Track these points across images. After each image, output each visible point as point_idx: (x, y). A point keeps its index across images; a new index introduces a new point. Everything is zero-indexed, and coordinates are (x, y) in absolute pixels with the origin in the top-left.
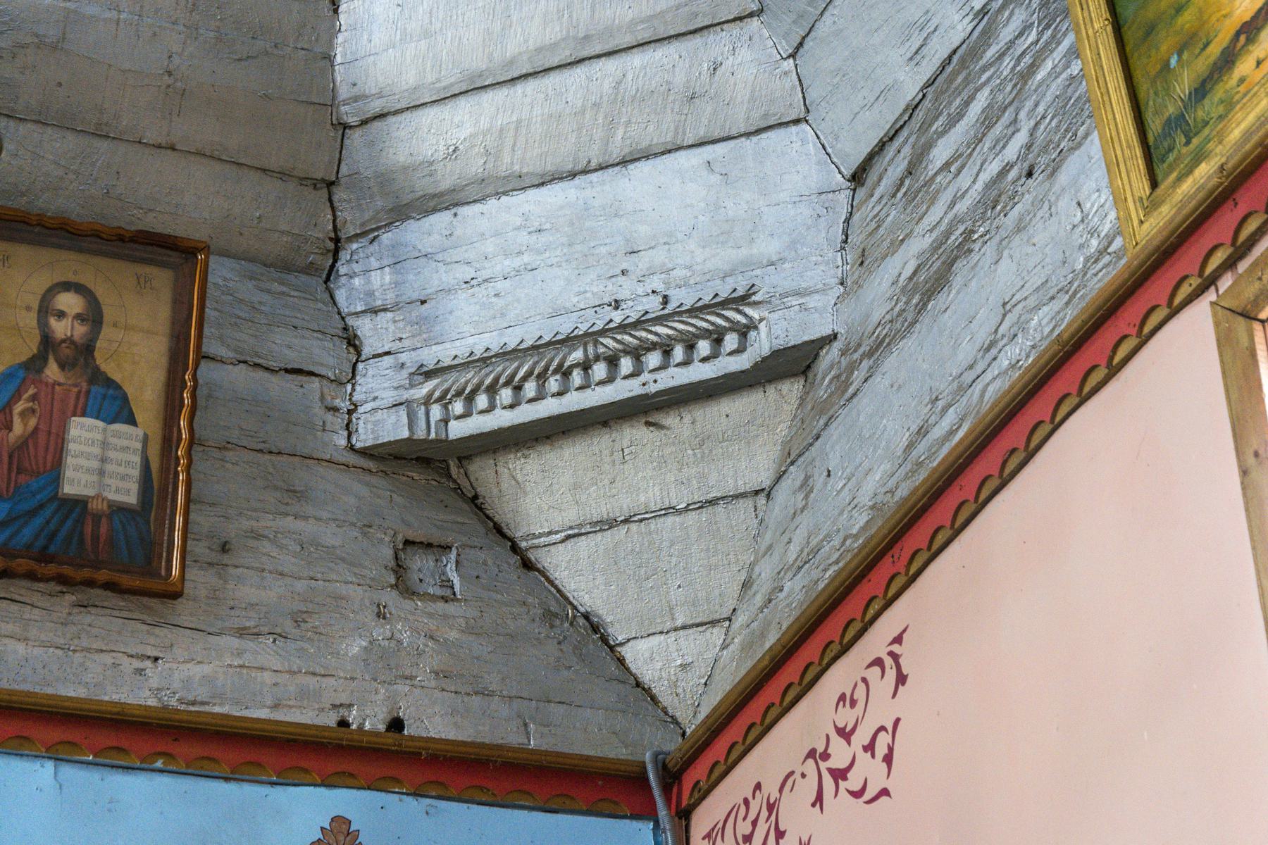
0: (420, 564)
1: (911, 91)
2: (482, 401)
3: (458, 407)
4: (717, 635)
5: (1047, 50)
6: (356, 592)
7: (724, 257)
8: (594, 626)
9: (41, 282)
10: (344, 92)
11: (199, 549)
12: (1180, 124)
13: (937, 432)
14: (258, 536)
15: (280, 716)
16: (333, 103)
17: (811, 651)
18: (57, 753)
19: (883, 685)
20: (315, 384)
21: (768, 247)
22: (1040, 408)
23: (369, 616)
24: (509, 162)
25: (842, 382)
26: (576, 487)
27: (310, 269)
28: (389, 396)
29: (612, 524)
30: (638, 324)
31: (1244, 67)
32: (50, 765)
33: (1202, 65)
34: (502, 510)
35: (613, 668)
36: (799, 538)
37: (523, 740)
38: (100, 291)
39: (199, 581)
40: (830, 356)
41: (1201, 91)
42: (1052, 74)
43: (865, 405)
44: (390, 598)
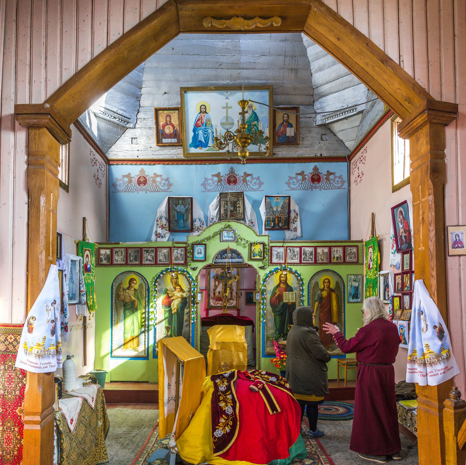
0: (324, 137)
2: (329, 119)
3: (327, 120)
4: (354, 141)
7: (353, 100)
9: (282, 114)
13: (372, 124)
14: (307, 136)
20: (312, 119)
21: (359, 99)
23: (318, 144)
24: (331, 91)
27: (311, 105)
28: (320, 119)
29: (343, 130)
32: (287, 164)
34: (332, 129)
35: (344, 146)
37: (333, 154)
38: (288, 114)
39: (301, 142)
40: (364, 111)
44: (321, 141)
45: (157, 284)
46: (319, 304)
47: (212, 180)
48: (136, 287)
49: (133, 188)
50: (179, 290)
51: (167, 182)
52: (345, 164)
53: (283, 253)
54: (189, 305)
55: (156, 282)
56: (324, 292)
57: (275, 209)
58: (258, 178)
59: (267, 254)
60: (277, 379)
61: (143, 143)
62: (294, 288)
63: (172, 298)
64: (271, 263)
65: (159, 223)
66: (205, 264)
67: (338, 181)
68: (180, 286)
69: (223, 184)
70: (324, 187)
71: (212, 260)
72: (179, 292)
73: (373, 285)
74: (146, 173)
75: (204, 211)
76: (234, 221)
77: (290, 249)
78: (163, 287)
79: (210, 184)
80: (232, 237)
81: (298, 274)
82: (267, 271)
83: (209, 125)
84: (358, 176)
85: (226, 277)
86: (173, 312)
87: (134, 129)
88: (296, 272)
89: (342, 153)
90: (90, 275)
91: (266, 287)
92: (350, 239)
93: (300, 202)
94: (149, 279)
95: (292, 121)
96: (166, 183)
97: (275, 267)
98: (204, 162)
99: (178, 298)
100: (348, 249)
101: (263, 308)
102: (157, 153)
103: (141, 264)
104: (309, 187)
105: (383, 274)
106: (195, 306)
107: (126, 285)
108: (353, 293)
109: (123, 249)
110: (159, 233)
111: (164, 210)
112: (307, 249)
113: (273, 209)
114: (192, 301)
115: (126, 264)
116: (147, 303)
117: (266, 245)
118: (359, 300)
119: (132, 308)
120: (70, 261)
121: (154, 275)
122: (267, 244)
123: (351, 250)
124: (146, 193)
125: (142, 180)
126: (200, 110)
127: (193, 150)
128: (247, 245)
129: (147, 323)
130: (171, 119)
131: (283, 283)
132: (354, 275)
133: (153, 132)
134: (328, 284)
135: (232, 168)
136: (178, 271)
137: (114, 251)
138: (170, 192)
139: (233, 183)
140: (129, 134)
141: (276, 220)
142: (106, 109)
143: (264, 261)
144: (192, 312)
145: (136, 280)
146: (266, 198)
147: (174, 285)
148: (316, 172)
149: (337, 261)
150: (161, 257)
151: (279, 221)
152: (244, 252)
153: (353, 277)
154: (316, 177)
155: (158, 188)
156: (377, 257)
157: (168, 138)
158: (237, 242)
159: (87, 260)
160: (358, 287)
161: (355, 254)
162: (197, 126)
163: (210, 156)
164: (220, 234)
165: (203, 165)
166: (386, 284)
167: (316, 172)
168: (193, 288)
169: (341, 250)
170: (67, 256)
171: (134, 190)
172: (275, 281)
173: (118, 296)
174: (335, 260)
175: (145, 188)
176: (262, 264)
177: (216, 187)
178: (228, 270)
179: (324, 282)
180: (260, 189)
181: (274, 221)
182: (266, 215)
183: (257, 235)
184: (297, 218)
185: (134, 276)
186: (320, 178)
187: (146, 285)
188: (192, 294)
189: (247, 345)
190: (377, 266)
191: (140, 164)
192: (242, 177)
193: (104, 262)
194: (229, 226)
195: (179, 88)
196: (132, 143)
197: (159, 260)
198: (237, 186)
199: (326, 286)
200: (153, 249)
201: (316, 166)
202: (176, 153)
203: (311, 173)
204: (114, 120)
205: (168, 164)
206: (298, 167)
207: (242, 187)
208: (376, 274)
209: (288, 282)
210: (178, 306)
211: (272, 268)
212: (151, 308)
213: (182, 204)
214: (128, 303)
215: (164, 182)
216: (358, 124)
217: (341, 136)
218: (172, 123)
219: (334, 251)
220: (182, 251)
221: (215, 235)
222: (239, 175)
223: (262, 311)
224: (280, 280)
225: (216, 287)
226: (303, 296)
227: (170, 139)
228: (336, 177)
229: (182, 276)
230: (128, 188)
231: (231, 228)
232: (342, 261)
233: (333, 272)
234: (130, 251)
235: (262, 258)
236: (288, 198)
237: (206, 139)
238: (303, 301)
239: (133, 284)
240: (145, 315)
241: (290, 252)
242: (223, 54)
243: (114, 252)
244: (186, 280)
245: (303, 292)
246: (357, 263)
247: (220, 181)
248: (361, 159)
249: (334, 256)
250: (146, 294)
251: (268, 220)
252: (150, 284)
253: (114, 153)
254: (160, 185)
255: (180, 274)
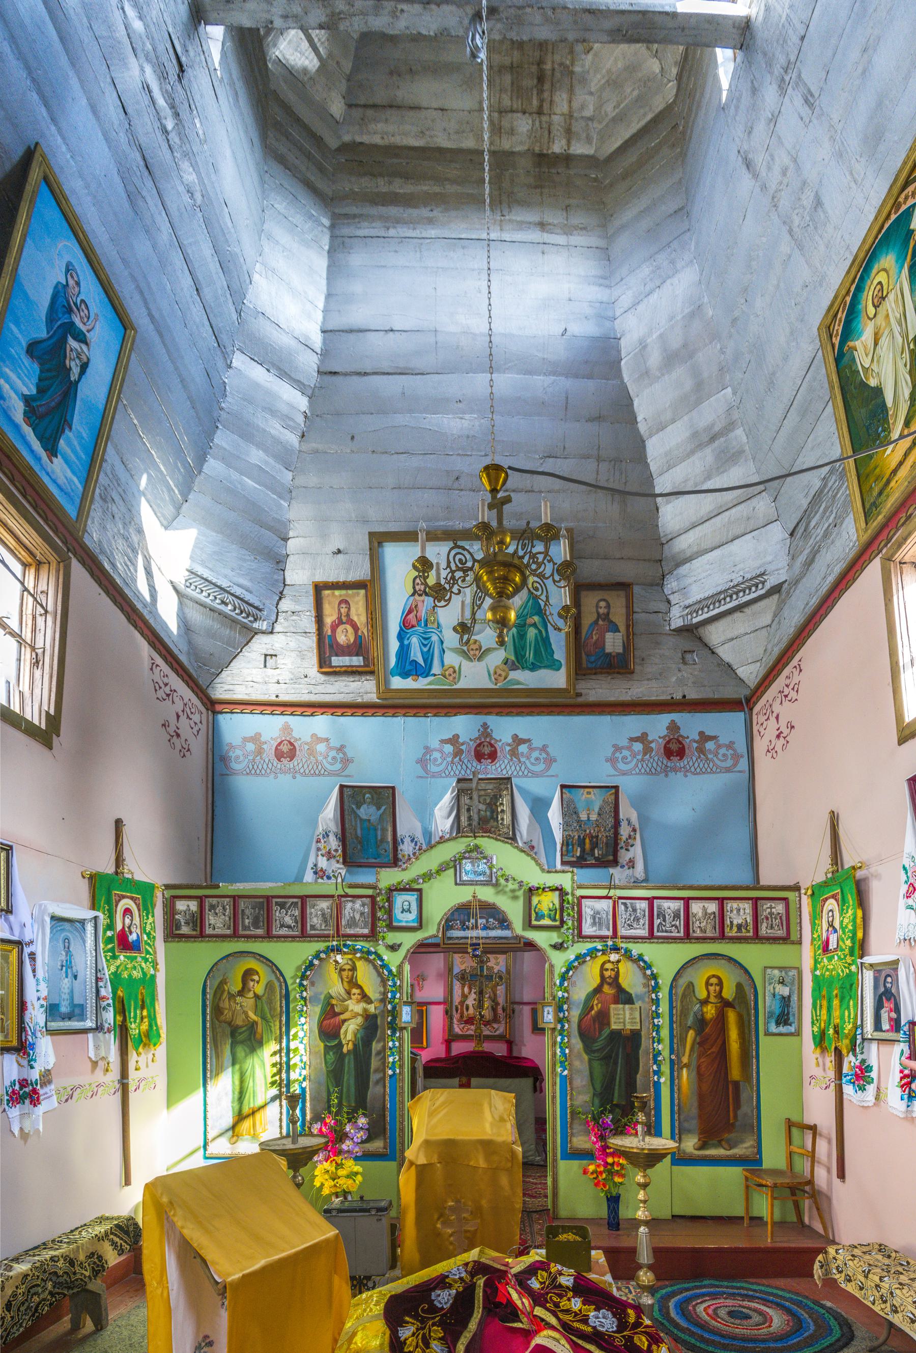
0: (688, 656)
1: (805, 507)
2: (700, 612)
3: (695, 615)
4: (758, 664)
5: (841, 487)
6: (674, 666)
8: (729, 666)
10: (662, 535)
11: (637, 661)
12: (875, 505)
13: (811, 604)
14: (649, 655)
15: (658, 698)
16: (659, 538)
17: (780, 666)
18: (610, 713)
19: (796, 672)
20: (661, 615)
21: (769, 558)
22: (836, 594)
25: (788, 593)
26: (724, 631)
27: (657, 585)
28: (678, 615)
29: (732, 639)
30: (737, 585)
31: (893, 484)
33: (881, 484)
34: (706, 640)
36: (777, 637)
39: (638, 668)
40: (785, 586)
41: (880, 493)
42: (843, 494)
43: (793, 598)
44: (681, 666)
45: (305, 983)
46: (696, 1035)
47: (441, 751)
48: (259, 989)
49: (265, 766)
50: (359, 997)
51: (341, 755)
52: (739, 717)
53: (607, 914)
54: (384, 1033)
55: (303, 977)
56: (709, 1007)
57: (583, 817)
58: (544, 749)
59: (569, 915)
60: (619, 1320)
61: (290, 666)
62: (637, 996)
63: (342, 1017)
64: (581, 936)
65: (321, 845)
66: (418, 936)
67: (724, 755)
68: (360, 987)
69: (466, 761)
70: (693, 769)
71: (435, 927)
72: (359, 1001)
73: (842, 993)
74: (295, 734)
75: (421, 821)
76: (489, 837)
77: (625, 904)
78: (320, 990)
79: (436, 760)
80: (484, 873)
81: (645, 962)
82: (570, 955)
83: (433, 623)
84: (778, 736)
85: (481, 976)
86: (345, 1050)
87: (271, 636)
88: (640, 958)
89: (729, 692)
90: (139, 959)
91: (567, 991)
92: (758, 882)
93: (640, 803)
94: (289, 971)
95: (619, 616)
96: (338, 757)
97: (589, 946)
98: (422, 712)
99: (356, 1015)
100: (765, 907)
101: (561, 1043)
102: (320, 689)
103: (269, 936)
104: (659, 769)
105: (871, 965)
106: (397, 1035)
107: (235, 985)
108: (777, 1011)
109: (228, 899)
110: (322, 870)
111: (331, 815)
112: (666, 904)
113: (578, 817)
114: (389, 1023)
115: (235, 935)
116: (284, 1029)
117: (567, 894)
118: (792, 1029)
119: (250, 1039)
120: (48, 919)
121: (300, 963)
122: (569, 890)
123: (771, 908)
124: (294, 778)
125: (285, 748)
126: (414, 588)
127: (397, 683)
128: (520, 893)
129: (284, 1076)
130: (349, 609)
131: (609, 984)
132: (780, 969)
133: (311, 642)
134: (718, 988)
135: (485, 726)
136: (355, 951)
137: (207, 904)
138: (346, 776)
139: (489, 758)
140: (260, 644)
141: (587, 841)
142: (192, 573)
143: (562, 930)
144: (391, 1049)
145: (258, 973)
146: (564, 790)
147: (345, 984)
148: (674, 735)
149: (739, 934)
150: (315, 920)
151: (594, 845)
152: (514, 911)
153: (776, 972)
154: (674, 747)
155: (320, 767)
156: (854, 920)
157: (343, 655)
158: (497, 885)
159: (127, 921)
160: (789, 997)
161: (781, 918)
162: (406, 625)
163: (435, 697)
164: (455, 867)
165: (421, 719)
166: (882, 989)
167: (674, 735)
168: (392, 991)
169: (747, 907)
170: (40, 905)
171: (268, 771)
172: (590, 976)
173: (218, 1011)
174: (734, 933)
175: (292, 766)
176: (559, 937)
177: (449, 768)
178: (475, 950)
179: (708, 984)
180: (550, 773)
181: (581, 843)
182: (564, 830)
183: (543, 870)
184: (635, 838)
185: (253, 964)
186: (684, 746)
187: (281, 986)
188: (389, 1007)
189: (520, 1149)
190: (853, 943)
191: (282, 714)
192: (509, 745)
193: (185, 930)
194: (477, 847)
195: (367, 537)
196: (265, 666)
197: (311, 926)
198: (498, 765)
199: (712, 994)
200: (295, 900)
201: (673, 721)
202: (362, 690)
203: (663, 738)
204: (222, 607)
205: (342, 715)
206: (634, 724)
207: (508, 767)
208: (850, 964)
209: (621, 980)
210: (355, 1035)
211: (583, 947)
212: (293, 1040)
213: (372, 802)
214: (241, 1027)
215: (333, 753)
216: (766, 619)
217: (725, 653)
218: (352, 620)
219: (731, 911)
220: (363, 905)
221: (442, 869)
222: (501, 740)
223: (558, 1051)
224: (602, 976)
225: (465, 997)
226: (658, 1016)
227: (347, 658)
228: (719, 746)
229: (366, 964)
230: (255, 767)
231: (481, 853)
232: (751, 934)
233: (730, 959)
234: (242, 904)
235: (558, 923)
236: (613, 791)
237: (426, 657)
238: (658, 1028)
239: (252, 984)
240: (281, 1057)
241: (626, 911)
242: (460, 452)
243: (207, 907)
244: (374, 972)
245: (658, 1006)
246: (785, 939)
247: (458, 753)
248: (786, 693)
249: (731, 922)
250: (281, 1007)
251: (566, 843)
252: (289, 982)
253: (226, 687)
254: (324, 761)
255: (360, 958)
